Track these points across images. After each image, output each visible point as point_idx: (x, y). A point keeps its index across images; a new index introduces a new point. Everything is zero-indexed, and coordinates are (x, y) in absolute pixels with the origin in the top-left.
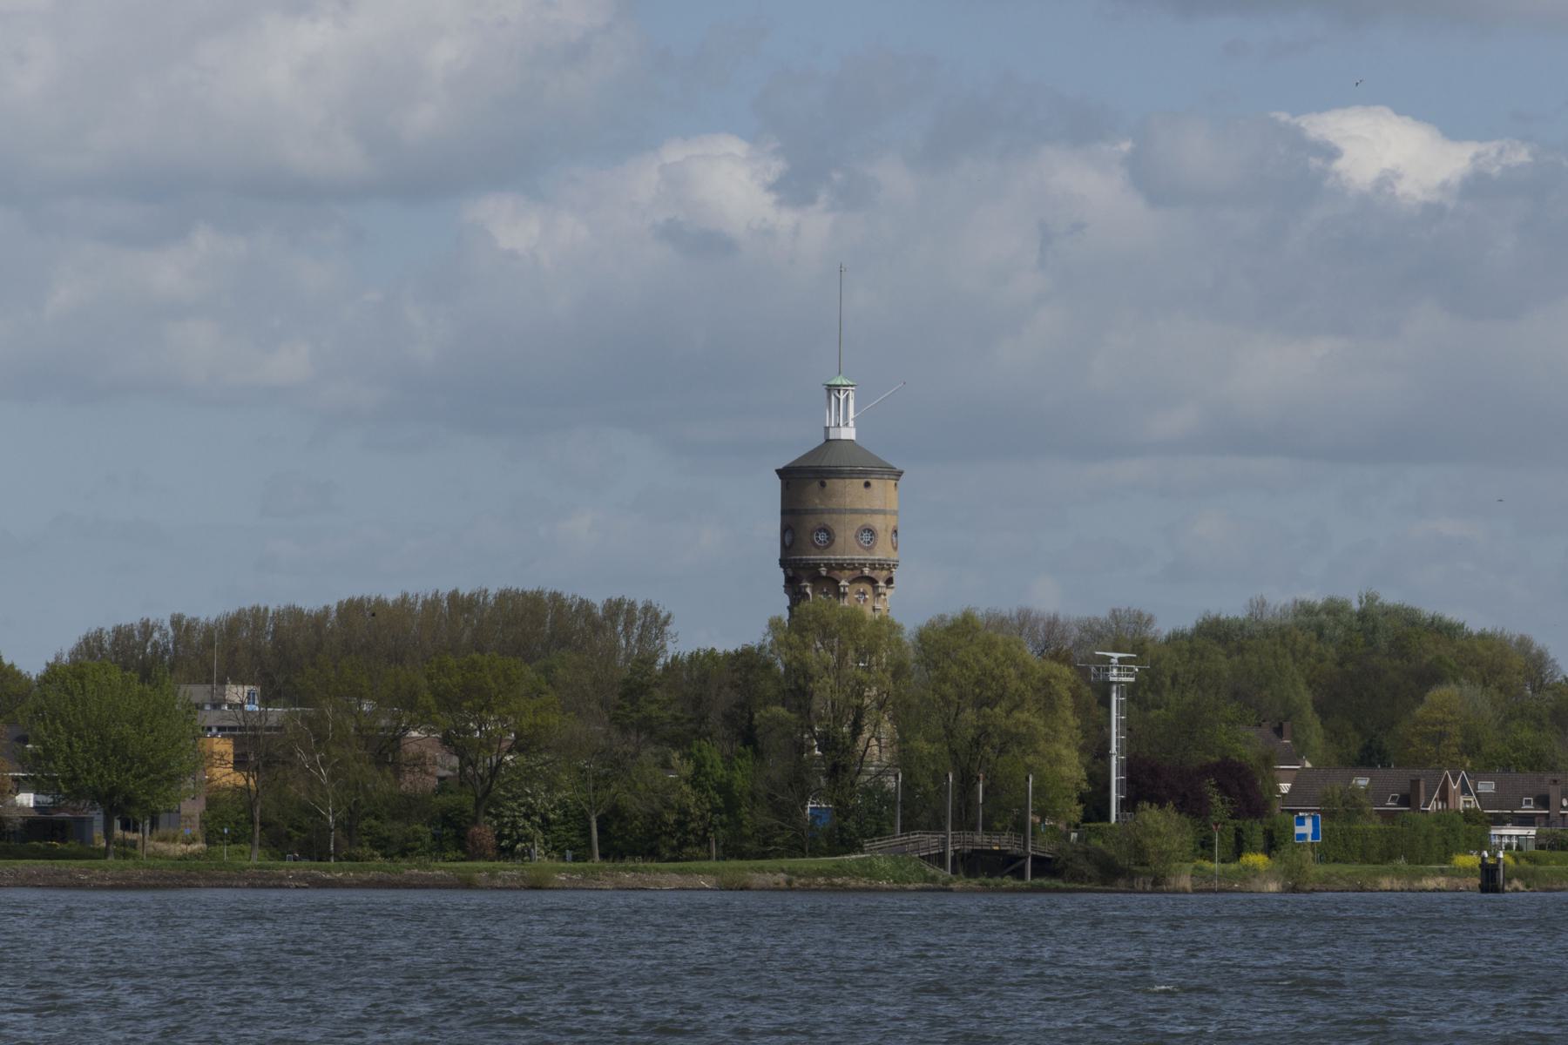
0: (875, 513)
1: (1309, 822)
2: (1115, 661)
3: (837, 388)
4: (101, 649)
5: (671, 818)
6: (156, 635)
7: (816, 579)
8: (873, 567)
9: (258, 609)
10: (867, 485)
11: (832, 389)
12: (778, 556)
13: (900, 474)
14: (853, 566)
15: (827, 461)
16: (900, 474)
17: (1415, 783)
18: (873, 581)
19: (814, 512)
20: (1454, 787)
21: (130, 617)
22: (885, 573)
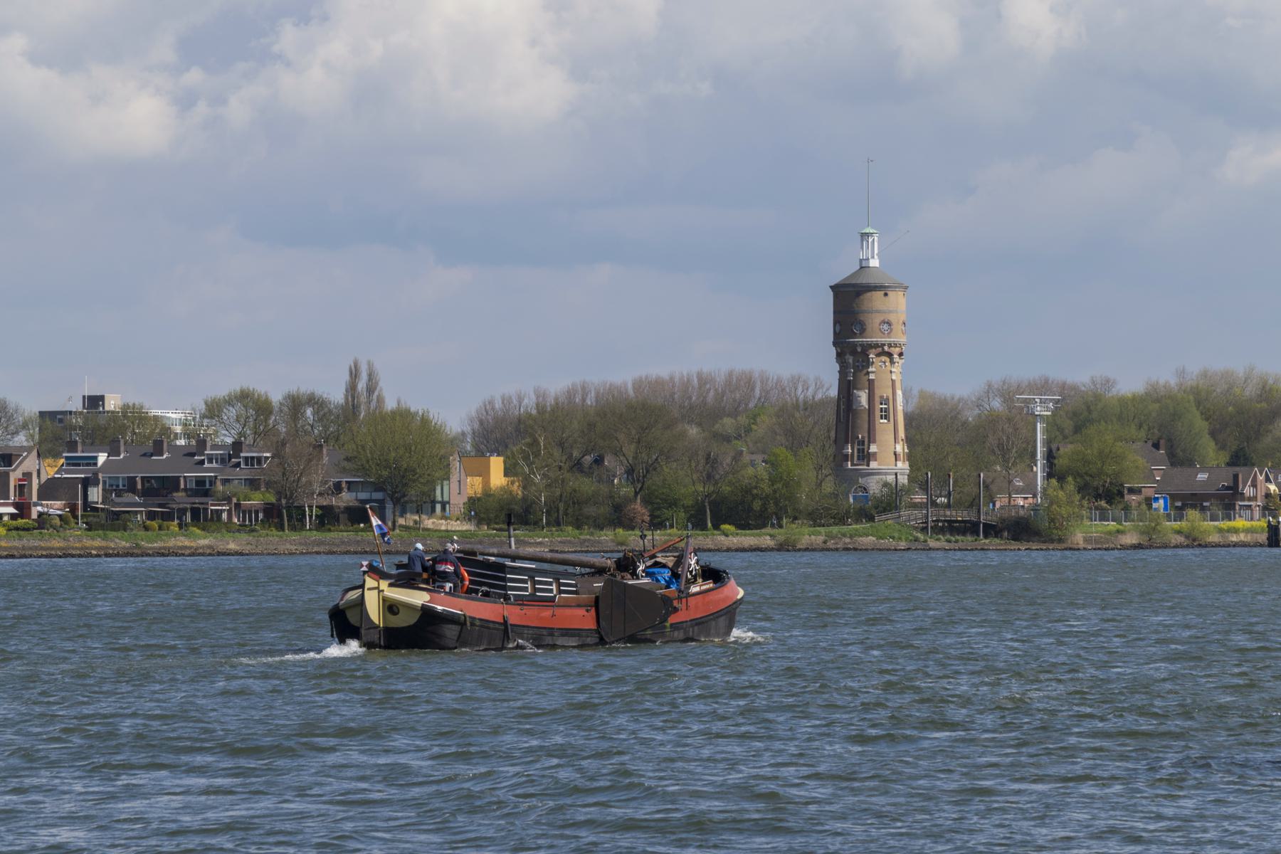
0: (894, 313)
1: (1161, 501)
2: (80, 448)
3: (868, 235)
4: (493, 409)
5: (757, 505)
6: (526, 401)
7: (854, 353)
8: (890, 346)
9: (128, 407)
10: (886, 295)
11: (865, 236)
12: (832, 339)
13: (906, 288)
14: (876, 346)
15: (864, 280)
16: (906, 288)
17: (1236, 477)
18: (890, 355)
19: (879, 312)
20: (1261, 478)
21: (511, 389)
22: (898, 350)
